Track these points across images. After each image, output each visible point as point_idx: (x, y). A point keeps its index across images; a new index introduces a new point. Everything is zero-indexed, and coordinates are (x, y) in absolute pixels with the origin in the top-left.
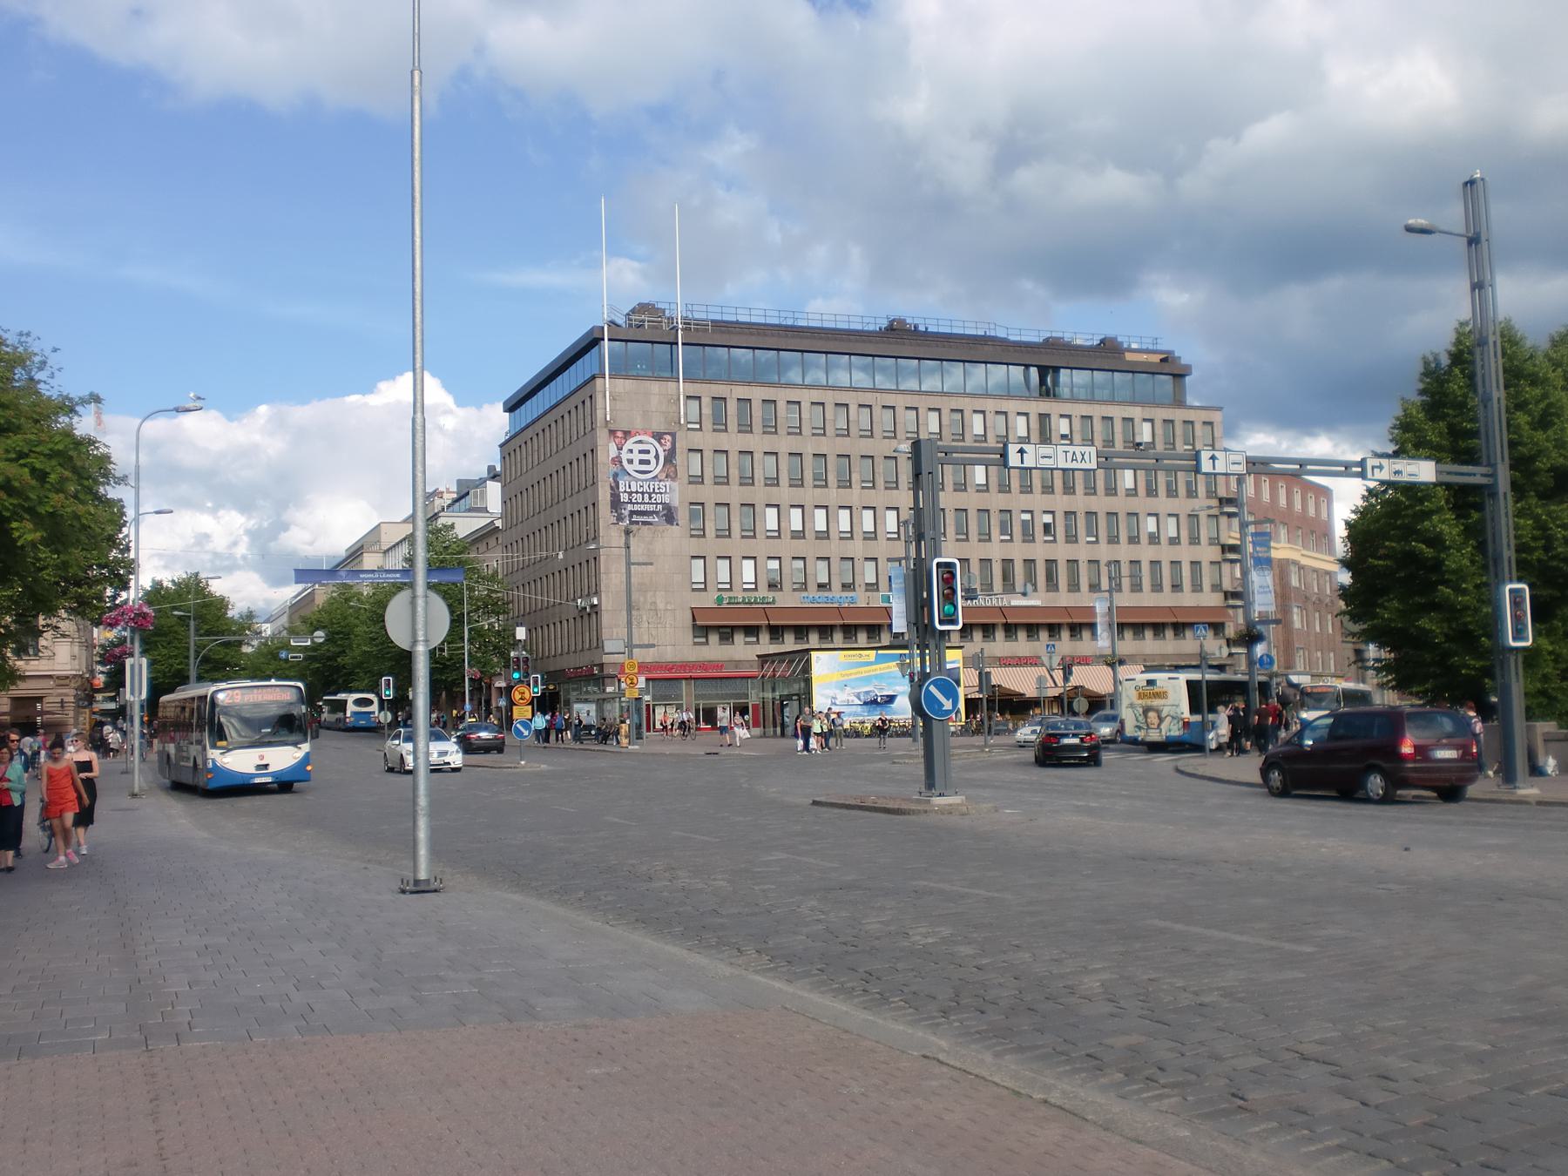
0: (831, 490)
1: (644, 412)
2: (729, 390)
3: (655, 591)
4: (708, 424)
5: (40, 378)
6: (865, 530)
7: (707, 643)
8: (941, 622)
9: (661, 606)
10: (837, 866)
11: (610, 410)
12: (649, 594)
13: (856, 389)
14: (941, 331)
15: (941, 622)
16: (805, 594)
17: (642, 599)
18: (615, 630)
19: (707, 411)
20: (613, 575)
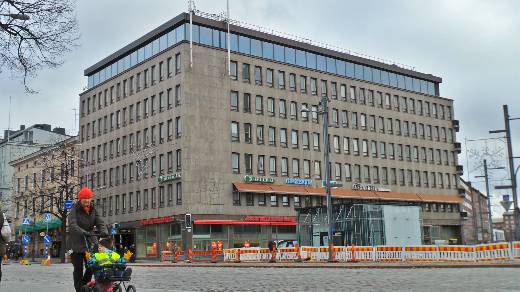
0: (276, 118)
1: (209, 66)
2: (251, 60)
3: (214, 172)
4: (240, 77)
5: (31, 30)
6: (281, 142)
7: (265, 205)
8: (187, 227)
9: (217, 181)
10: (513, 283)
11: (193, 62)
12: (211, 173)
13: (242, 54)
14: (370, 59)
15: (187, 227)
16: (287, 179)
17: (207, 176)
18: (192, 194)
19: (240, 70)
20: (192, 160)
